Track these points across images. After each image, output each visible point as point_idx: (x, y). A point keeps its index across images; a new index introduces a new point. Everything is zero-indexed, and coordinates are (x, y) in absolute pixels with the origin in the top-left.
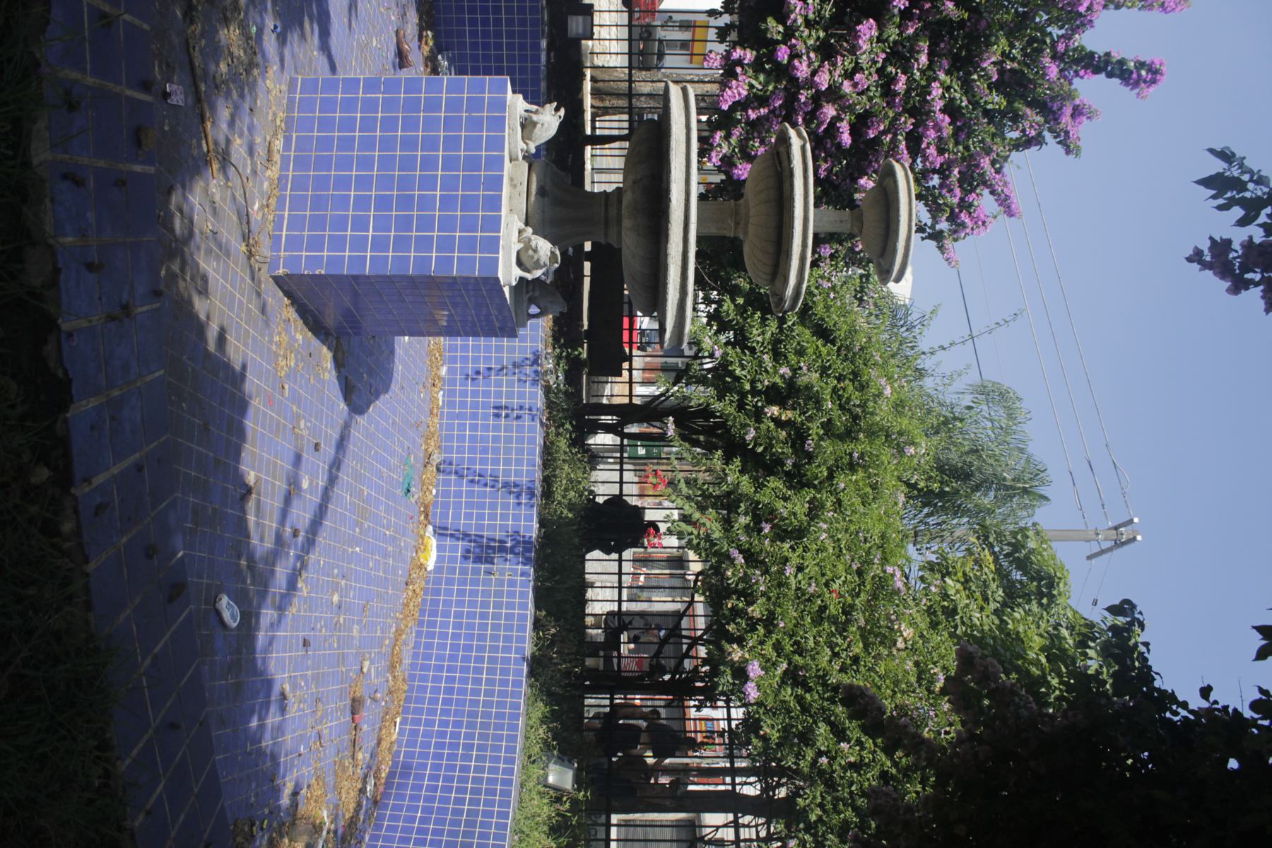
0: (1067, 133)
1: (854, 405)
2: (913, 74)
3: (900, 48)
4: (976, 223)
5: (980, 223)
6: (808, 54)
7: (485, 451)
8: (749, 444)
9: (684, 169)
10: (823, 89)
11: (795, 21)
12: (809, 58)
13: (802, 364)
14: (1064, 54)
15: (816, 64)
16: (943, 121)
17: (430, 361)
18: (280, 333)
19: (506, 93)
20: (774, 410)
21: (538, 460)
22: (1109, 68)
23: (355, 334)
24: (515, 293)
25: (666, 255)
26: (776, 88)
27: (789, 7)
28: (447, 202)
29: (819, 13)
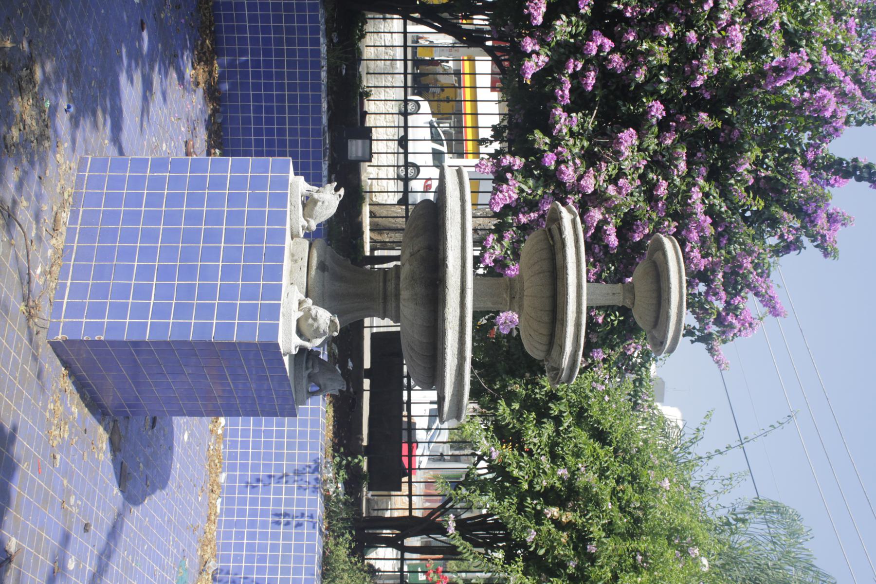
0: (823, 236)
1: (634, 508)
2: (673, 180)
3: (660, 158)
4: (743, 325)
5: (747, 324)
6: (574, 160)
7: (262, 559)
8: (530, 547)
9: (460, 238)
10: (590, 192)
11: (560, 131)
12: (575, 163)
13: (580, 465)
14: (814, 162)
15: (582, 170)
16: (705, 221)
17: (210, 466)
18: (55, 402)
19: (288, 172)
20: (554, 511)
21: (317, 570)
22: (858, 173)
23: (133, 413)
24: (295, 365)
25: (444, 320)
26: (544, 192)
27: (554, 118)
28: (229, 272)
29: (583, 127)
